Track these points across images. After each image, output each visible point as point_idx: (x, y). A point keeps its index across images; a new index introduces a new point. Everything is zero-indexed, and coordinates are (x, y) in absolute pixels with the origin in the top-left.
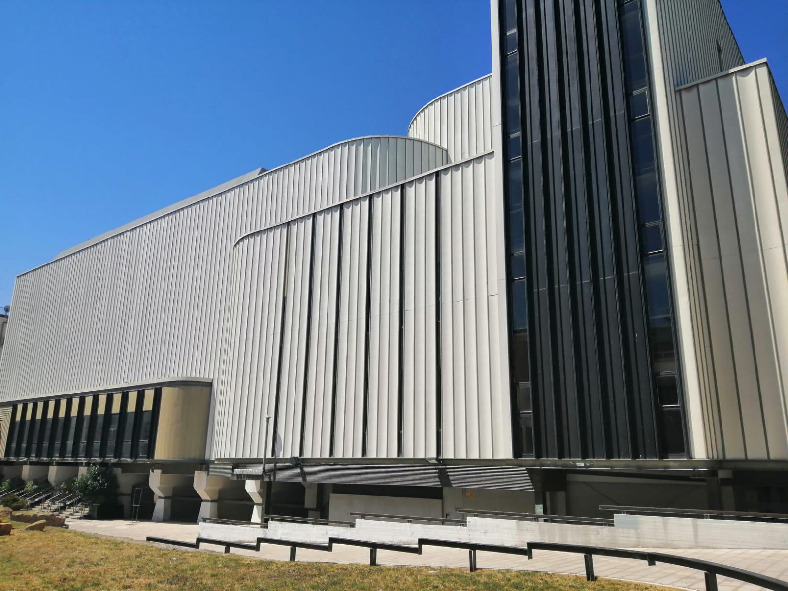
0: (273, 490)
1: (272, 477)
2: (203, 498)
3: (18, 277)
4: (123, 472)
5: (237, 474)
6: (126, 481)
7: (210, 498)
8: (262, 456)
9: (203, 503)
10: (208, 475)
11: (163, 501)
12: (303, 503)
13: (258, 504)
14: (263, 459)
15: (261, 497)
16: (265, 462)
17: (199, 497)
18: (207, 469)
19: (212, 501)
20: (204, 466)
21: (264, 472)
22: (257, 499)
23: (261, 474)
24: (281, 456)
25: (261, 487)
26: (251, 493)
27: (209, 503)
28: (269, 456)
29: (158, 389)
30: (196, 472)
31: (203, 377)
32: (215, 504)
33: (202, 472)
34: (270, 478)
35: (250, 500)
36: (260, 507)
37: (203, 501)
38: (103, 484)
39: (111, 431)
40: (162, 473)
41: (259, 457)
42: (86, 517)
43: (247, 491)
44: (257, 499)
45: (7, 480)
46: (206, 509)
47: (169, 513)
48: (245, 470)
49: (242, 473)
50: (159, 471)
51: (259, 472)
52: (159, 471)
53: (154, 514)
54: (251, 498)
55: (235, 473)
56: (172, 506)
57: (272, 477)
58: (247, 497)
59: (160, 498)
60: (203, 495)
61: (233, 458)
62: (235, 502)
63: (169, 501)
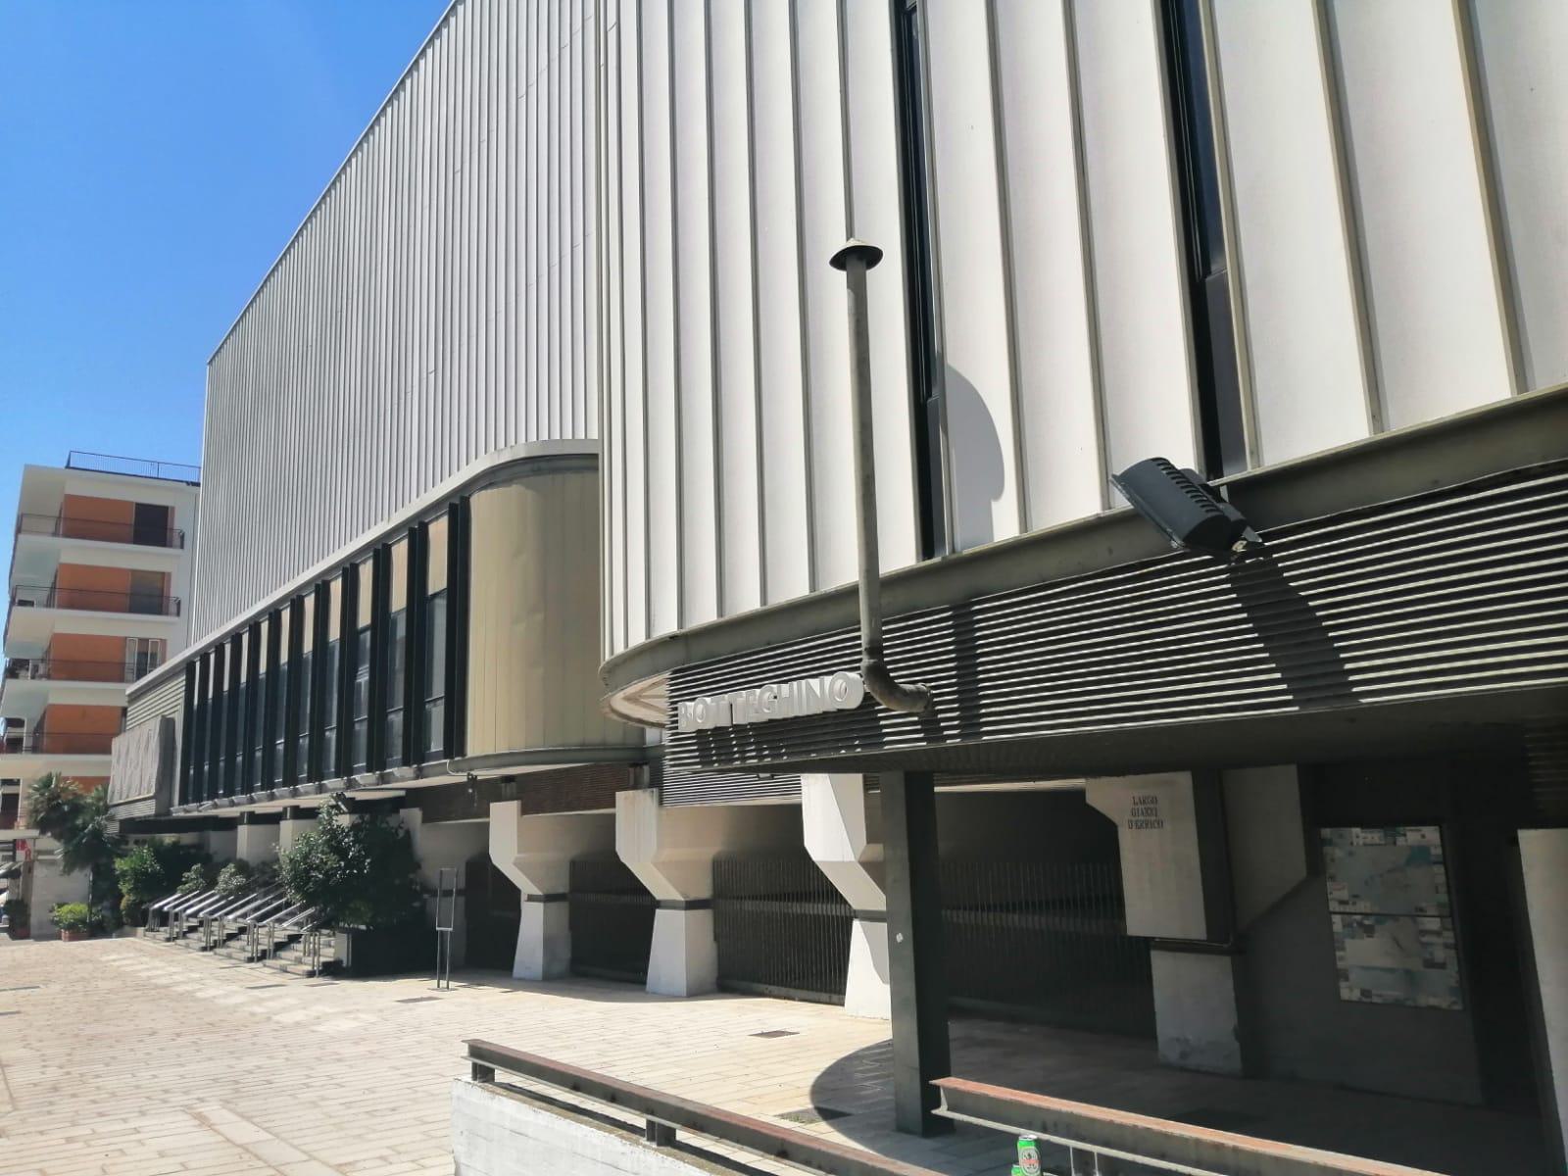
0: (944, 846)
1: (949, 716)
2: (658, 895)
3: (210, 363)
4: (426, 820)
5: (701, 734)
6: (436, 848)
7: (682, 894)
8: (846, 571)
9: (658, 912)
10: (661, 802)
11: (539, 906)
12: (1113, 901)
13: (870, 916)
14: (851, 593)
15: (880, 881)
16: (873, 611)
17: (643, 891)
18: (656, 782)
19: (691, 905)
20: (646, 768)
21: (878, 674)
22: (861, 892)
23: (853, 702)
24: (1005, 527)
25: (871, 839)
26: (825, 863)
27: (681, 914)
28: (900, 552)
29: (457, 509)
30: (620, 796)
31: (583, 437)
32: (705, 916)
33: (639, 793)
34: (930, 726)
35: (832, 894)
36: (882, 928)
37: (658, 904)
38: (356, 863)
39: (360, 684)
40: (525, 810)
41: (831, 583)
42: (332, 971)
43: (814, 859)
44: (861, 892)
45: (194, 867)
46: (676, 941)
47: (565, 953)
48: (742, 697)
49: (724, 722)
50: (513, 806)
51: (838, 690)
52: (513, 806)
53: (517, 958)
54: (646, 889)
55: (686, 726)
56: (574, 925)
57: (949, 716)
58: (814, 884)
59: (531, 898)
60: (659, 886)
61: (673, 638)
62: (775, 907)
63: (561, 910)
